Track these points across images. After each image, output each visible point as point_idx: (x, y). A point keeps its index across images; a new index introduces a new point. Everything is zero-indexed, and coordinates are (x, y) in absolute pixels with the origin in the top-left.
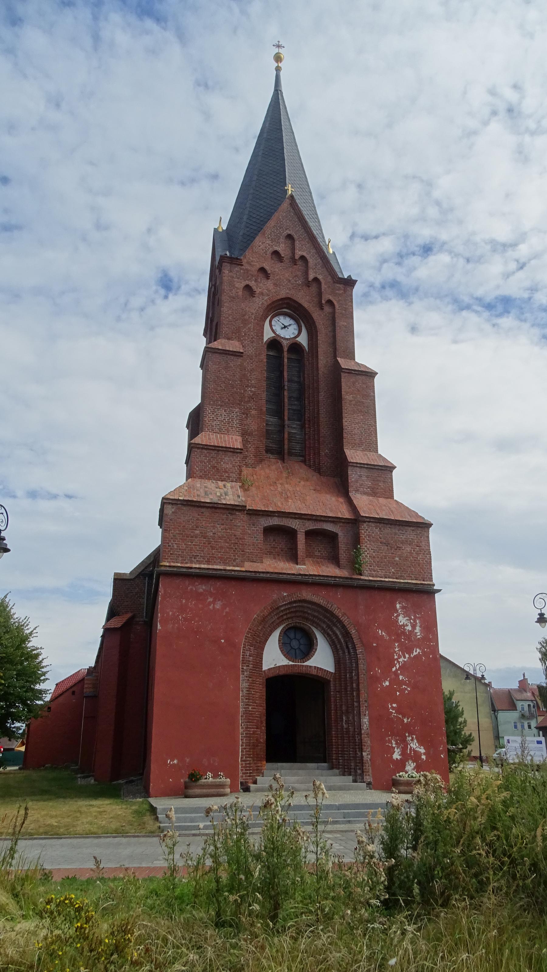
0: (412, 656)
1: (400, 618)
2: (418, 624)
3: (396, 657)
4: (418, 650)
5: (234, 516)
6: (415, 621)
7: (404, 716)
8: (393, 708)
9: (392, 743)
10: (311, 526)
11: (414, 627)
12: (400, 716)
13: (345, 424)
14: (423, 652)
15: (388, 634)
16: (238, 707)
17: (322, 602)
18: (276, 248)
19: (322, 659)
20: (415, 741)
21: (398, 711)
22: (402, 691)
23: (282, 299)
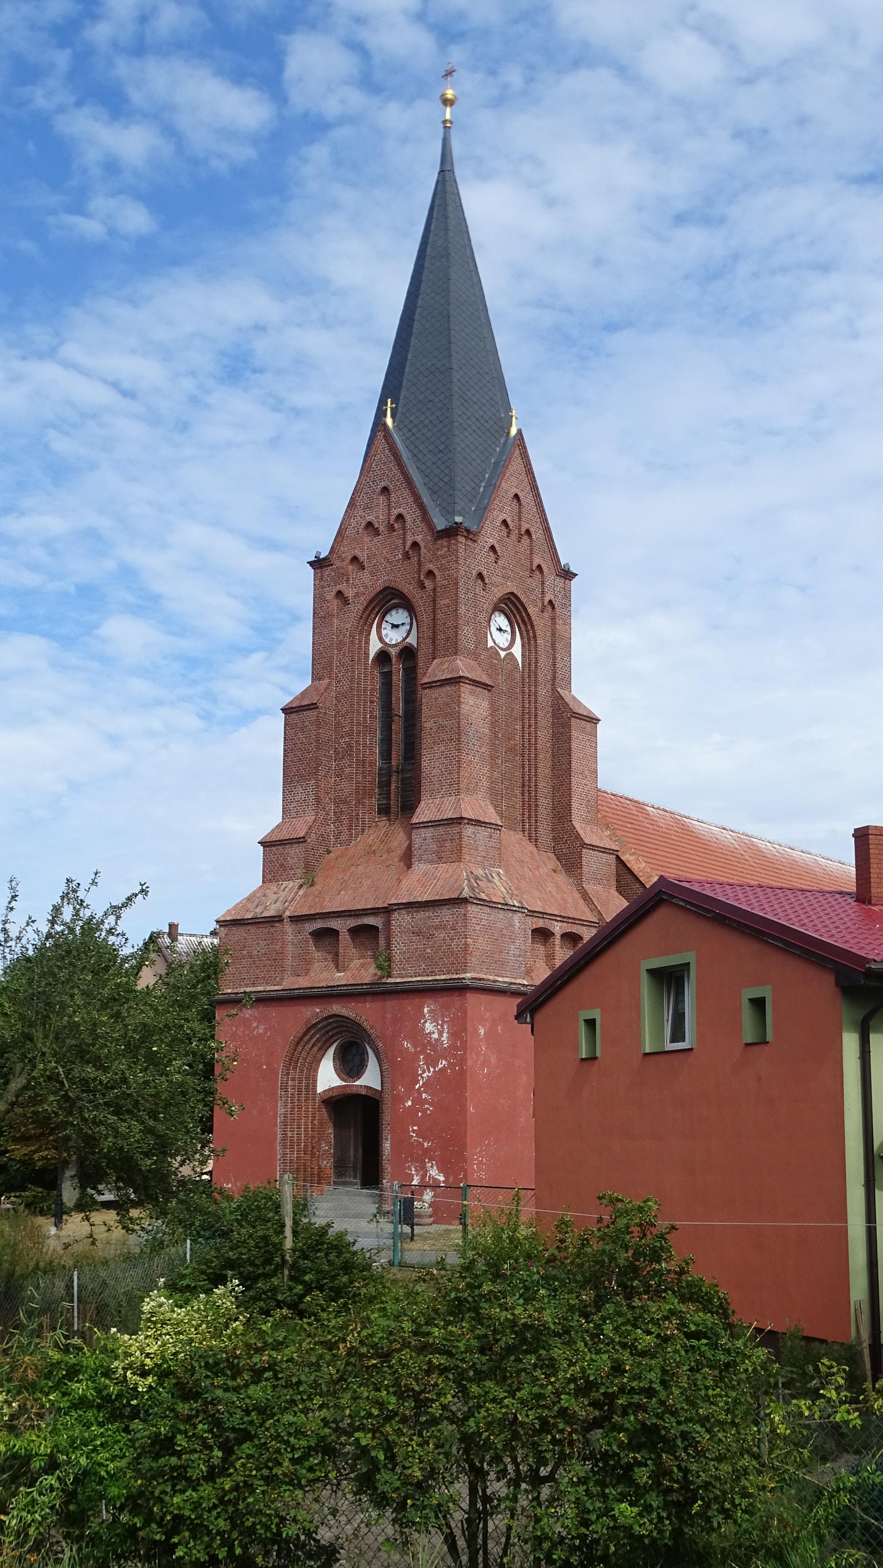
0: (437, 1069)
1: (427, 1025)
2: (446, 1030)
3: (420, 1072)
4: (444, 1062)
5: (275, 929)
6: (442, 1027)
7: (424, 1140)
8: (414, 1131)
9: (411, 1170)
10: (352, 923)
11: (441, 1034)
12: (421, 1140)
13: (424, 764)
14: (449, 1063)
15: (414, 1046)
16: (276, 1134)
17: (351, 1015)
18: (369, 518)
19: (370, 1078)
20: (435, 1167)
21: (419, 1134)
22: (424, 1111)
23: (381, 592)
